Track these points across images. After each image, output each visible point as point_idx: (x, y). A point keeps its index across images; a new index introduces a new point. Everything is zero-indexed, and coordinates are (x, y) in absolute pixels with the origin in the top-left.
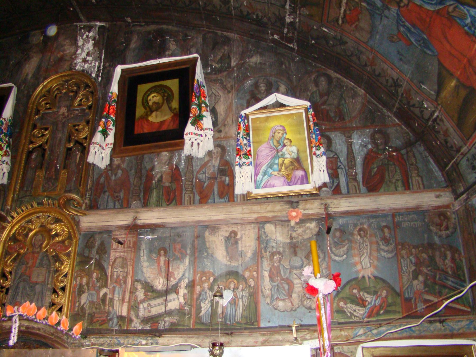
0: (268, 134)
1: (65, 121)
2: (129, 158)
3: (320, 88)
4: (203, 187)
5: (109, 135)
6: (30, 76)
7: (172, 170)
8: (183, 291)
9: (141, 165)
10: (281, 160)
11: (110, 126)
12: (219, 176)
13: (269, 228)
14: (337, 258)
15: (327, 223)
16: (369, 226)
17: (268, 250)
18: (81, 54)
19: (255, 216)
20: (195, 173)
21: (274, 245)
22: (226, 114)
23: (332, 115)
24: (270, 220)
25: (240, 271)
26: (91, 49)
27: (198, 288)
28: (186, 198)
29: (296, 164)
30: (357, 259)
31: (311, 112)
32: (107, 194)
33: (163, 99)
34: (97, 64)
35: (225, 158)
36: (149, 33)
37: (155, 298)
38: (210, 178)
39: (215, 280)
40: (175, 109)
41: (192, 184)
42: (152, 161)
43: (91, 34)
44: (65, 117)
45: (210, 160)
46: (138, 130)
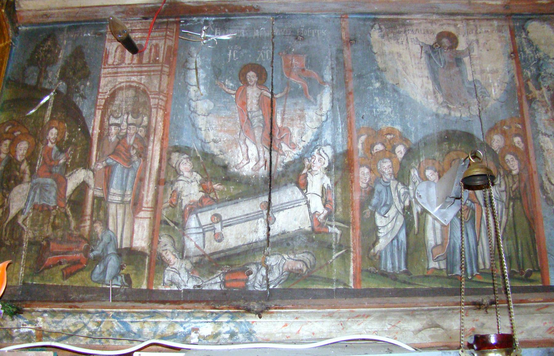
8: (318, 181)
25: (477, 132)
27: (363, 175)
37: (233, 199)
39: (411, 153)
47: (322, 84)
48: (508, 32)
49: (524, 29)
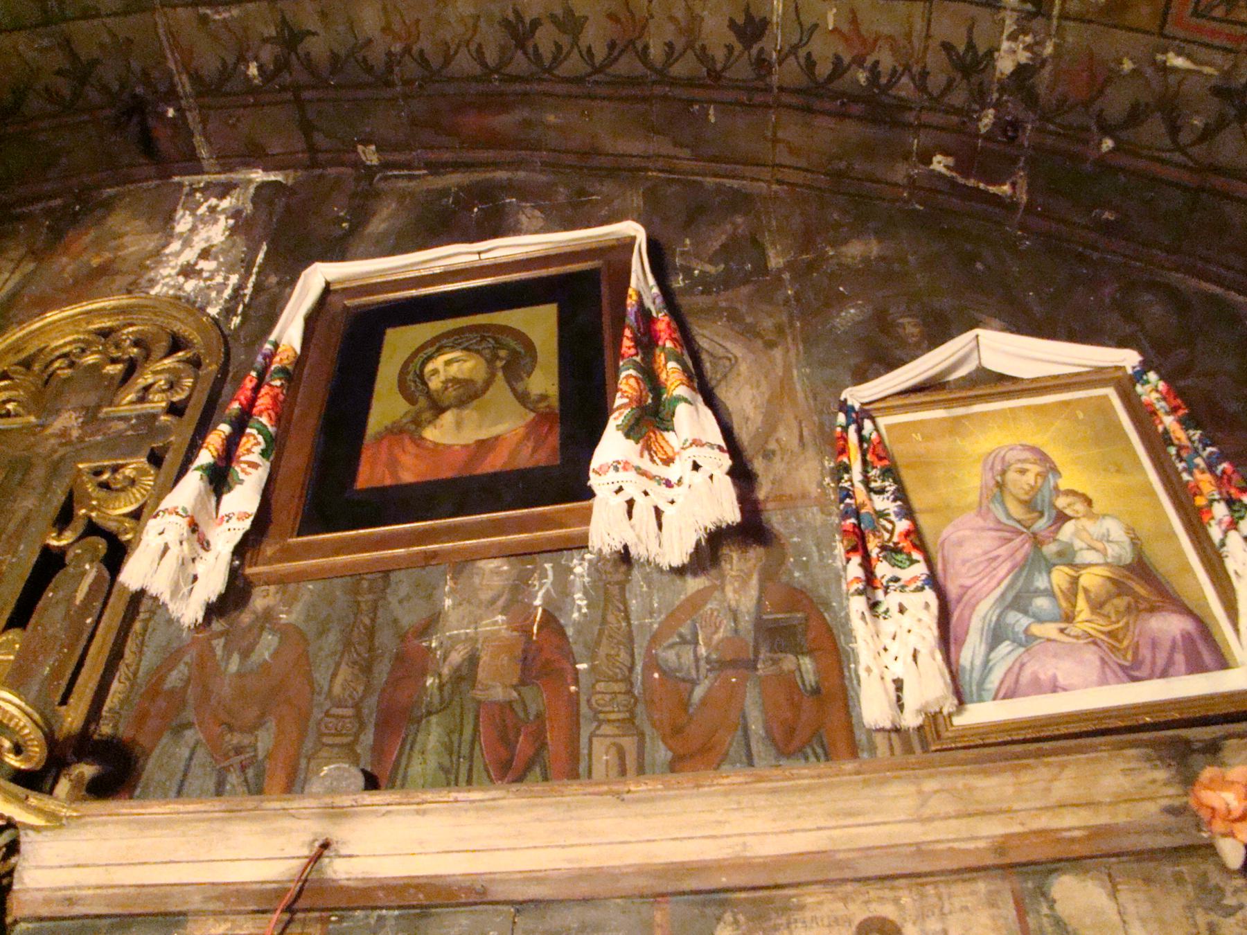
0: (973, 481)
1: (62, 458)
2: (320, 584)
3: (1149, 325)
4: (685, 705)
5: (241, 482)
7: (527, 632)
9: (375, 609)
10: (1060, 577)
11: (249, 451)
12: (764, 654)
18: (177, 254)
19: (994, 828)
22: (767, 415)
24: (1078, 850)
28: (602, 756)
32: (190, 735)
34: (234, 279)
35: (784, 578)
36: (445, 192)
38: (720, 665)
40: (543, 397)
41: (629, 692)
42: (429, 593)
45: (713, 588)
48: (1011, 905)
49: (1044, 895)
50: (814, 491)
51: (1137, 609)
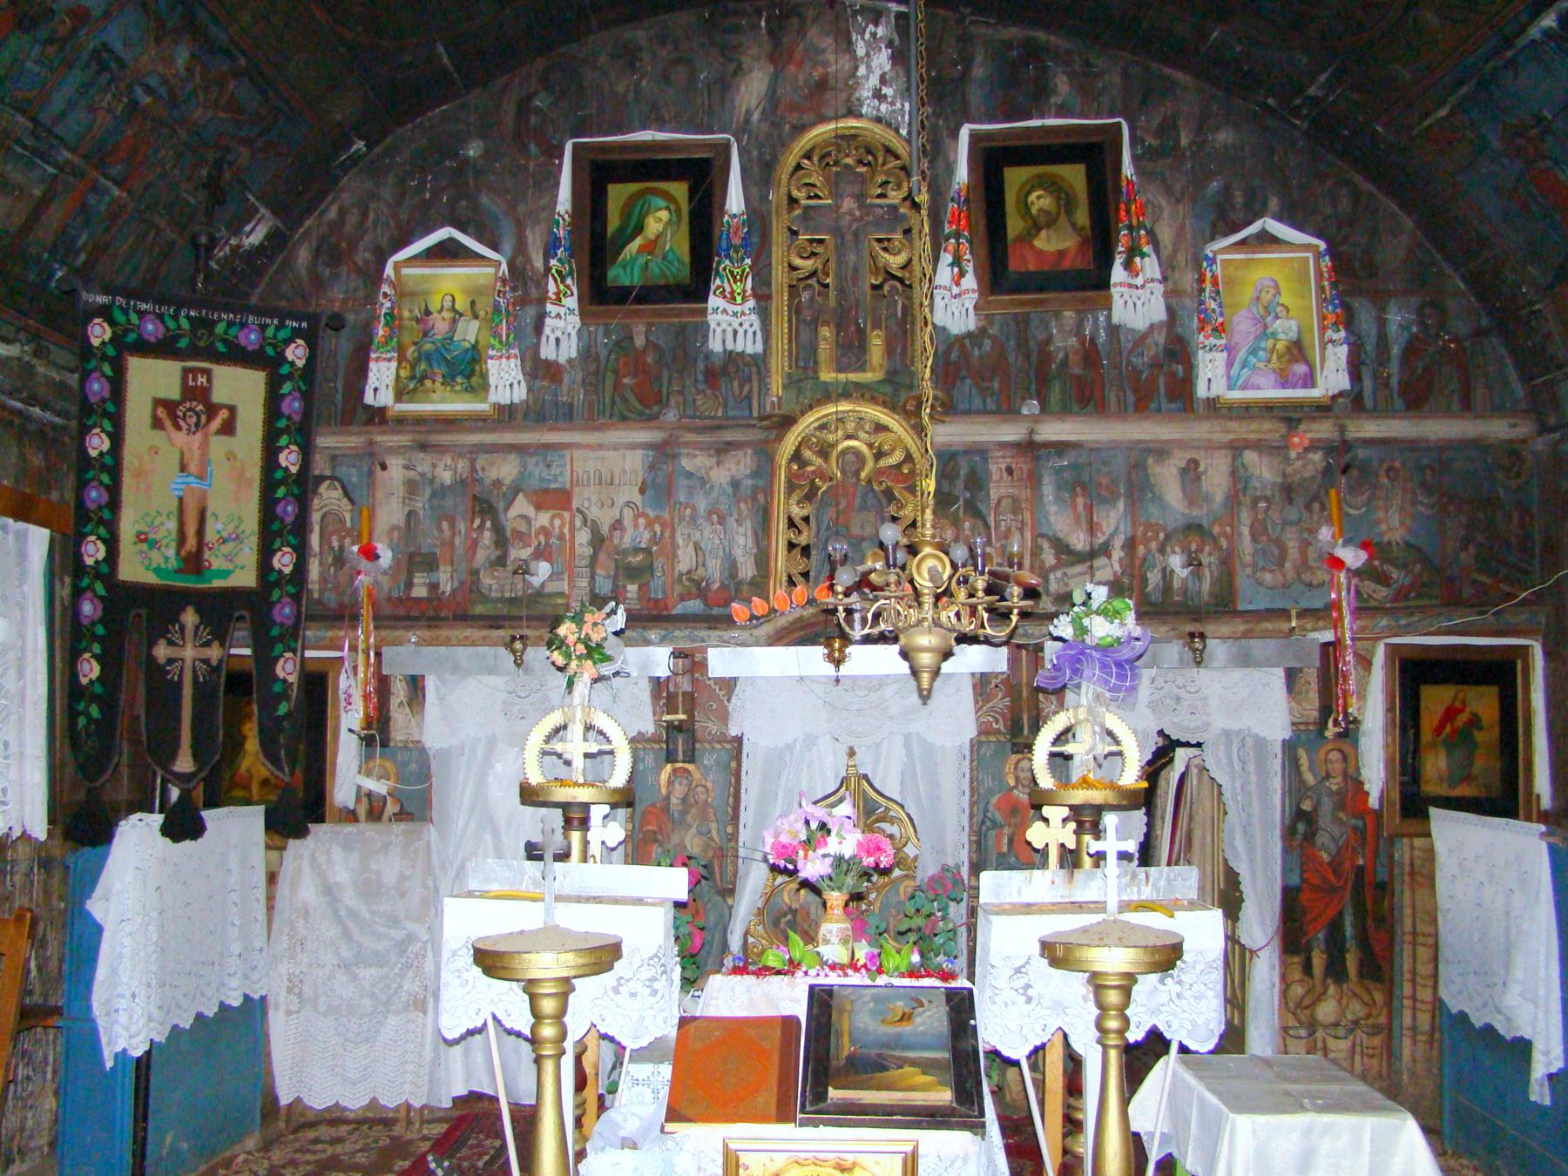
0: (1248, 293)
4: (1139, 379)
6: (756, 116)
8: (1117, 554)
10: (1270, 343)
13: (1250, 457)
14: (1351, 511)
15: (1344, 461)
16: (1403, 464)
17: (1249, 492)
18: (867, 77)
19: (1232, 437)
20: (1125, 354)
21: (1258, 485)
23: (1357, 265)
25: (1205, 524)
26: (887, 67)
27: (1141, 550)
29: (1295, 352)
30: (1381, 514)
31: (1326, 262)
32: (968, 382)
33: (1059, 206)
36: (1008, 45)
37: (1072, 564)
39: (1167, 536)
43: (880, 31)
44: (855, 220)
46: (1014, 265)
47: (1118, 497)
50: (1189, 289)
51: (1294, 360)
